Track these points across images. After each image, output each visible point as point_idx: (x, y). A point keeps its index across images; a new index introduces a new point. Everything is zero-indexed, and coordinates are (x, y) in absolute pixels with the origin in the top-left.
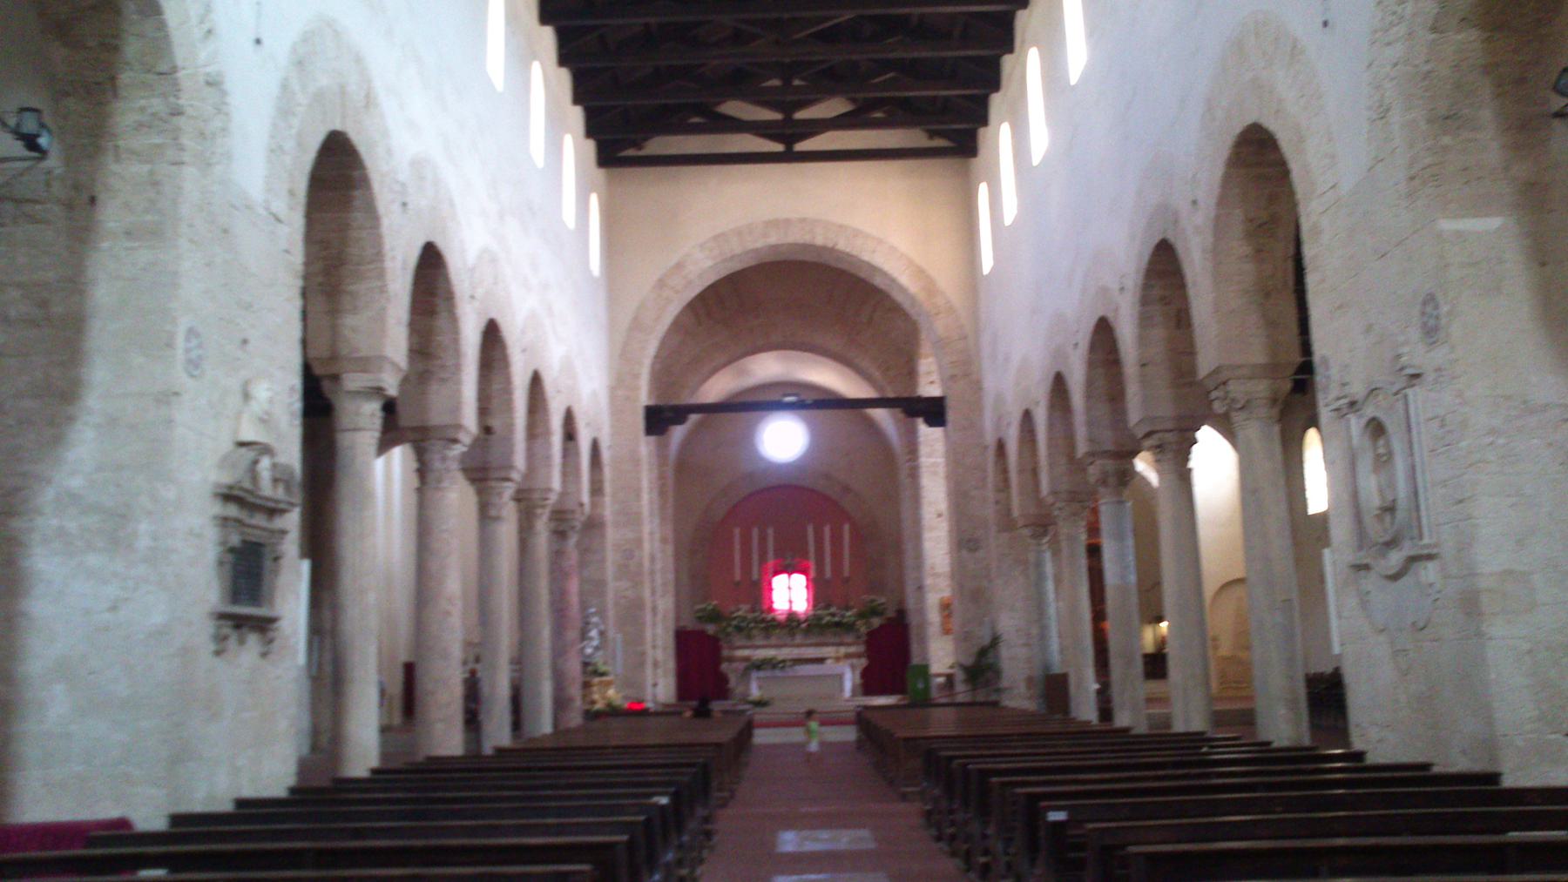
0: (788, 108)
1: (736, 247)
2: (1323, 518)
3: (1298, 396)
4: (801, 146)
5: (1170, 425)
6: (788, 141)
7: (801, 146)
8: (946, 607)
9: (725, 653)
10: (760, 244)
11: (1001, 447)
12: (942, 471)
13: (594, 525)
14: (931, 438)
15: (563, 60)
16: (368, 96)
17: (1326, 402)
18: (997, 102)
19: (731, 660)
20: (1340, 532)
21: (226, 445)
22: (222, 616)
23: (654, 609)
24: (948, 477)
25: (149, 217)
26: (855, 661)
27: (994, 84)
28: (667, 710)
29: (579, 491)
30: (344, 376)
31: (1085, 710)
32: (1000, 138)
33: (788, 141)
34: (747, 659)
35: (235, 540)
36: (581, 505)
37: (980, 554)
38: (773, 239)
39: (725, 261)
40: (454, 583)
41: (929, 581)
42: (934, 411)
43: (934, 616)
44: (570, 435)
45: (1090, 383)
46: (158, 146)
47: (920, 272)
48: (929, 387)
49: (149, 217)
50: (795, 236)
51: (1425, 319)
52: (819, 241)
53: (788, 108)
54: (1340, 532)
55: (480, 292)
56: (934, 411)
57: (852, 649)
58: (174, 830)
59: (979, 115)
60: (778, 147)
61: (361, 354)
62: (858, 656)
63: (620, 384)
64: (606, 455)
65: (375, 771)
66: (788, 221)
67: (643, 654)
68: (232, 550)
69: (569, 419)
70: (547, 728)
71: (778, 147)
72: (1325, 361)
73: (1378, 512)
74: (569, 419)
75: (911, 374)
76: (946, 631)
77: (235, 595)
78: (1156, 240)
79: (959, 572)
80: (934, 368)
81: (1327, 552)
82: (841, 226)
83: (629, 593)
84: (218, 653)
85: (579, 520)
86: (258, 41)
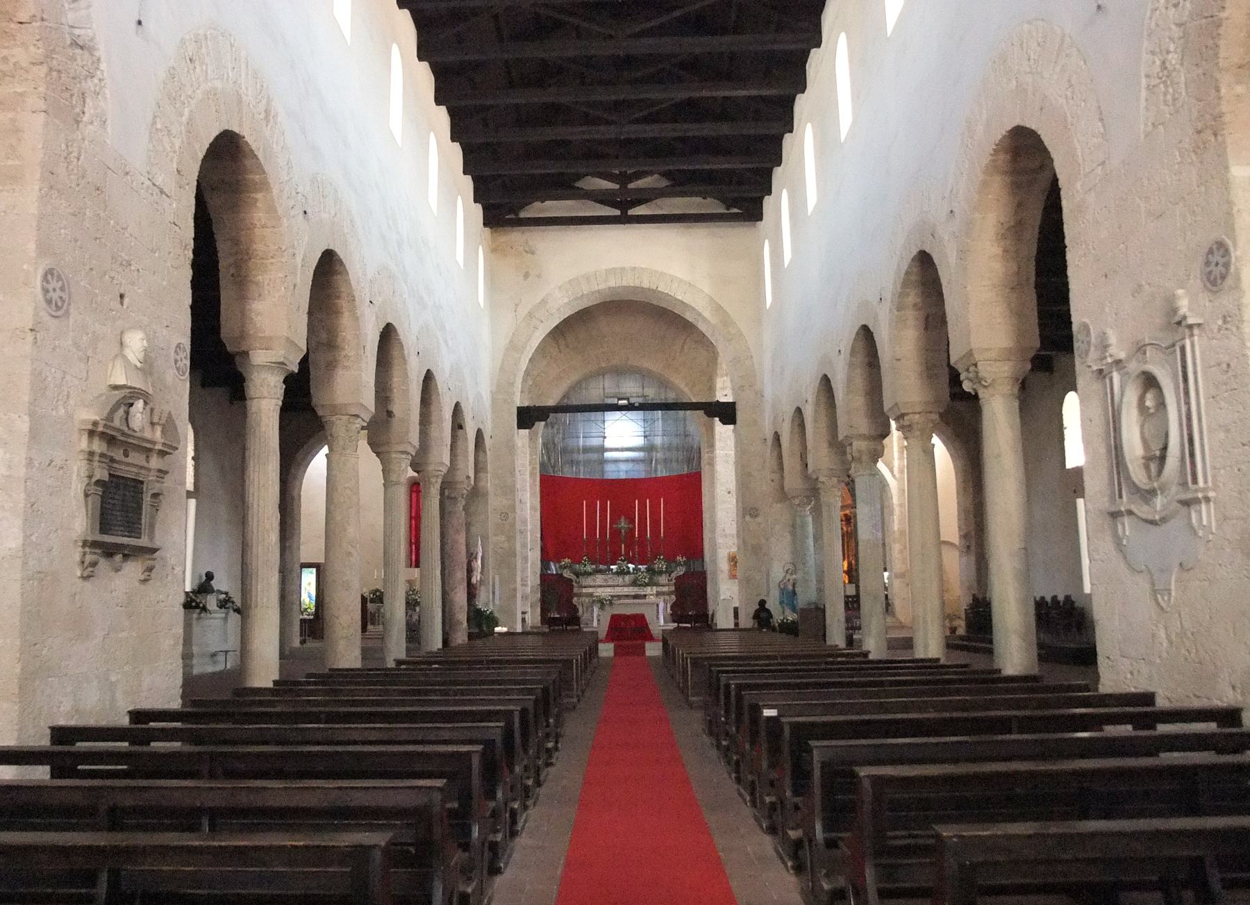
0: (624, 179)
1: (586, 289)
2: (1078, 471)
3: (1042, 375)
4: (633, 212)
5: (918, 410)
6: (624, 205)
7: (631, 212)
8: (733, 560)
9: (575, 590)
10: (602, 286)
11: (777, 438)
12: (732, 459)
13: (476, 493)
14: (723, 432)
15: (423, 52)
16: (267, 112)
17: (1085, 363)
18: (778, 174)
19: (579, 595)
20: (1095, 484)
21: (103, 389)
22: (95, 544)
23: (525, 559)
24: (736, 463)
25: (10, 162)
26: (667, 597)
27: (800, 84)
28: (535, 630)
29: (467, 467)
30: (250, 352)
31: (836, 637)
32: (779, 204)
33: (624, 205)
34: (591, 595)
35: (101, 474)
36: (468, 477)
37: (759, 519)
38: (613, 283)
39: (577, 299)
40: (123, 467)
41: (720, 540)
42: (727, 413)
43: (724, 566)
44: (458, 425)
45: (850, 380)
46: (21, 94)
47: (718, 309)
48: (724, 394)
49: (10, 162)
50: (629, 281)
51: (1224, 260)
52: (646, 285)
53: (624, 179)
54: (1095, 484)
55: (378, 301)
56: (727, 413)
57: (665, 589)
58: (133, 726)
59: (765, 186)
60: (617, 212)
61: (267, 334)
62: (669, 594)
63: (501, 389)
64: (488, 442)
65: (275, 682)
66: (623, 269)
67: (515, 590)
68: (98, 483)
69: (457, 410)
70: (437, 644)
71: (617, 212)
72: (1086, 327)
73: (1143, 461)
74: (457, 410)
75: (711, 389)
76: (733, 577)
77: (105, 525)
78: (915, 252)
79: (743, 531)
80: (728, 384)
81: (1080, 502)
82: (661, 273)
83: (506, 545)
84: (85, 578)
85: (464, 488)
86: (140, 23)
